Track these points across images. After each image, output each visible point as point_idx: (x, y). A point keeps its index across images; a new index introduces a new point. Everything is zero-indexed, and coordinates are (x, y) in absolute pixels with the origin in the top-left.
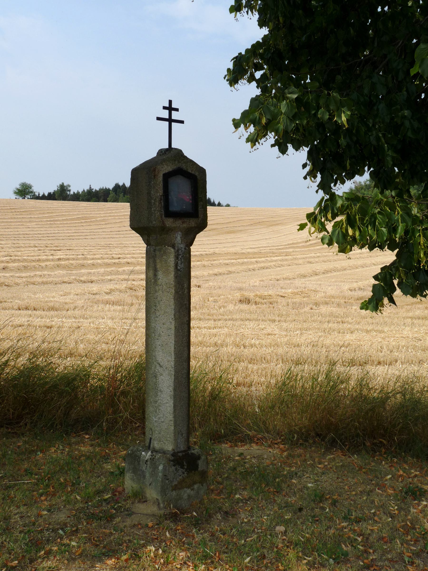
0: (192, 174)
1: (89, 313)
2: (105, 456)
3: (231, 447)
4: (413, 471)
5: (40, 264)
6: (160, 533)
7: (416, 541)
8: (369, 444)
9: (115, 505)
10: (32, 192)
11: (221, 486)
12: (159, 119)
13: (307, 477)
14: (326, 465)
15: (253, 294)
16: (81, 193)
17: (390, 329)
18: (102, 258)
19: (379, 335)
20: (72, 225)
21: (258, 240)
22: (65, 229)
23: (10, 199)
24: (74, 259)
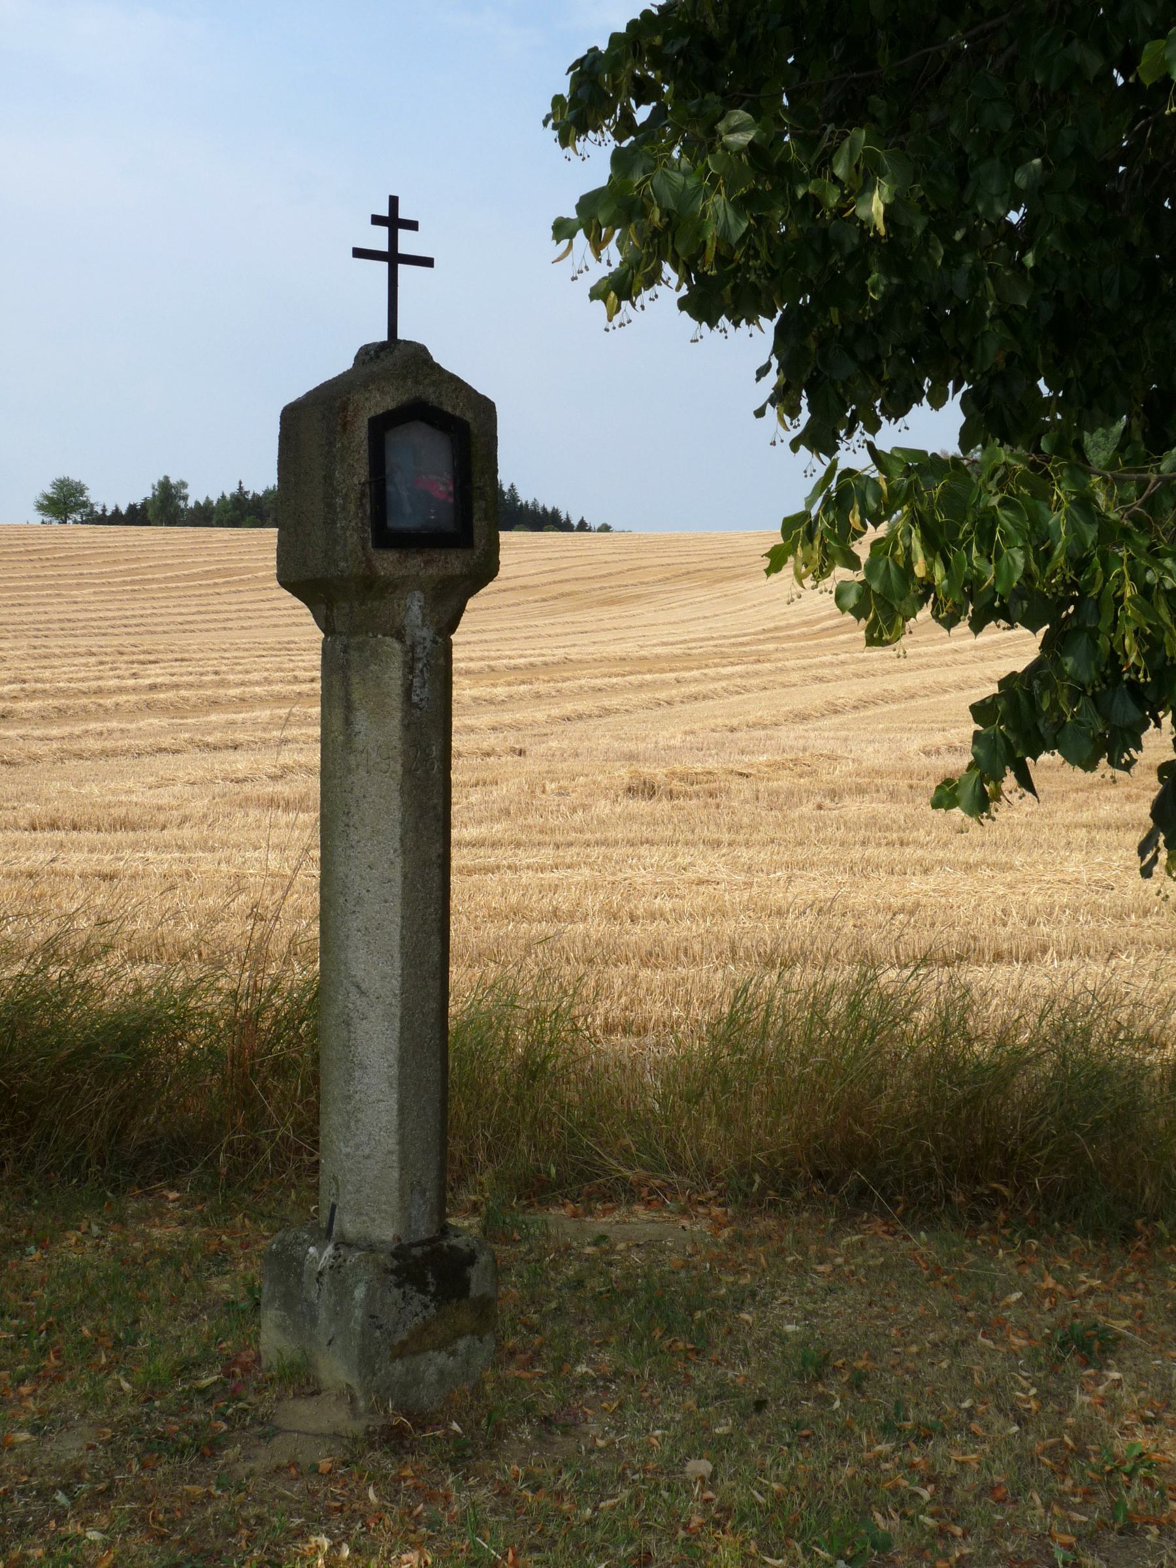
0: (453, 417)
1: (218, 833)
2: (216, 1254)
3: (575, 1215)
4: (1082, 1277)
5: (101, 701)
6: (352, 1490)
7: (1089, 1493)
8: (962, 1198)
9: (228, 1407)
10: (84, 504)
11: (537, 1340)
12: (359, 253)
13: (784, 1303)
14: (839, 1266)
15: (665, 771)
16: (215, 503)
17: (1029, 860)
18: (268, 681)
19: (999, 876)
20: (191, 592)
21: (683, 621)
22: (171, 604)
23: (28, 526)
24: (191, 686)
